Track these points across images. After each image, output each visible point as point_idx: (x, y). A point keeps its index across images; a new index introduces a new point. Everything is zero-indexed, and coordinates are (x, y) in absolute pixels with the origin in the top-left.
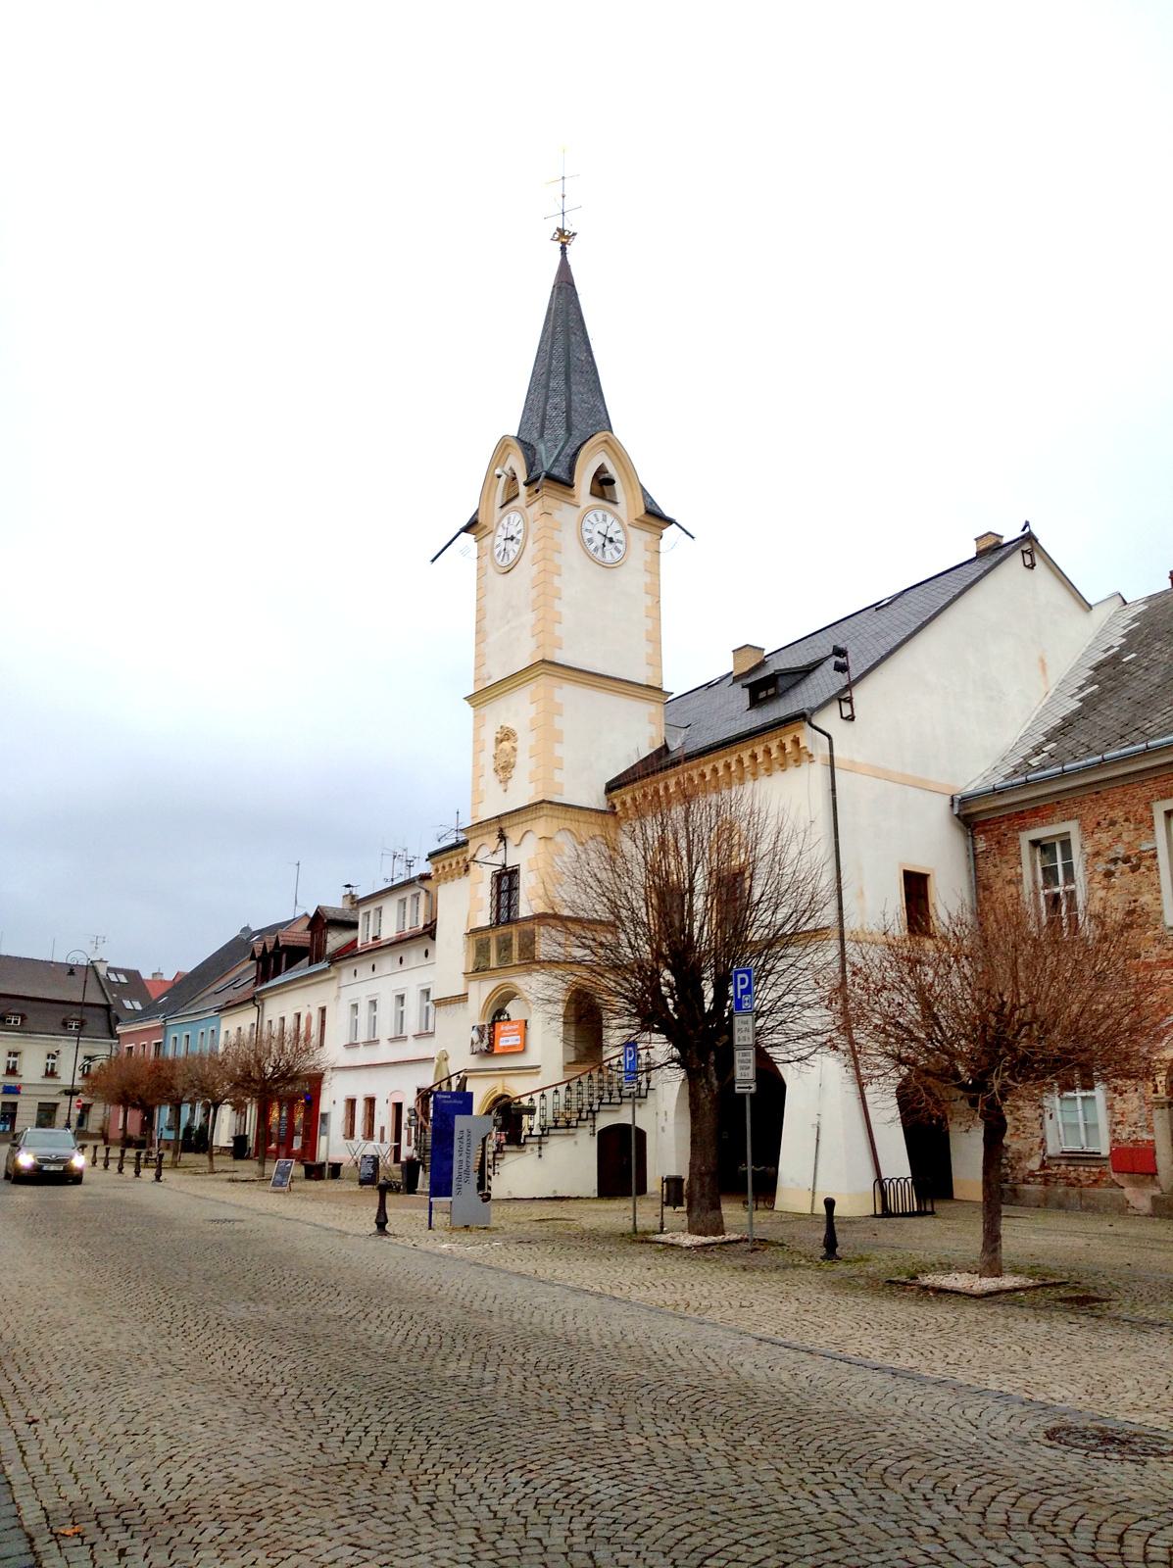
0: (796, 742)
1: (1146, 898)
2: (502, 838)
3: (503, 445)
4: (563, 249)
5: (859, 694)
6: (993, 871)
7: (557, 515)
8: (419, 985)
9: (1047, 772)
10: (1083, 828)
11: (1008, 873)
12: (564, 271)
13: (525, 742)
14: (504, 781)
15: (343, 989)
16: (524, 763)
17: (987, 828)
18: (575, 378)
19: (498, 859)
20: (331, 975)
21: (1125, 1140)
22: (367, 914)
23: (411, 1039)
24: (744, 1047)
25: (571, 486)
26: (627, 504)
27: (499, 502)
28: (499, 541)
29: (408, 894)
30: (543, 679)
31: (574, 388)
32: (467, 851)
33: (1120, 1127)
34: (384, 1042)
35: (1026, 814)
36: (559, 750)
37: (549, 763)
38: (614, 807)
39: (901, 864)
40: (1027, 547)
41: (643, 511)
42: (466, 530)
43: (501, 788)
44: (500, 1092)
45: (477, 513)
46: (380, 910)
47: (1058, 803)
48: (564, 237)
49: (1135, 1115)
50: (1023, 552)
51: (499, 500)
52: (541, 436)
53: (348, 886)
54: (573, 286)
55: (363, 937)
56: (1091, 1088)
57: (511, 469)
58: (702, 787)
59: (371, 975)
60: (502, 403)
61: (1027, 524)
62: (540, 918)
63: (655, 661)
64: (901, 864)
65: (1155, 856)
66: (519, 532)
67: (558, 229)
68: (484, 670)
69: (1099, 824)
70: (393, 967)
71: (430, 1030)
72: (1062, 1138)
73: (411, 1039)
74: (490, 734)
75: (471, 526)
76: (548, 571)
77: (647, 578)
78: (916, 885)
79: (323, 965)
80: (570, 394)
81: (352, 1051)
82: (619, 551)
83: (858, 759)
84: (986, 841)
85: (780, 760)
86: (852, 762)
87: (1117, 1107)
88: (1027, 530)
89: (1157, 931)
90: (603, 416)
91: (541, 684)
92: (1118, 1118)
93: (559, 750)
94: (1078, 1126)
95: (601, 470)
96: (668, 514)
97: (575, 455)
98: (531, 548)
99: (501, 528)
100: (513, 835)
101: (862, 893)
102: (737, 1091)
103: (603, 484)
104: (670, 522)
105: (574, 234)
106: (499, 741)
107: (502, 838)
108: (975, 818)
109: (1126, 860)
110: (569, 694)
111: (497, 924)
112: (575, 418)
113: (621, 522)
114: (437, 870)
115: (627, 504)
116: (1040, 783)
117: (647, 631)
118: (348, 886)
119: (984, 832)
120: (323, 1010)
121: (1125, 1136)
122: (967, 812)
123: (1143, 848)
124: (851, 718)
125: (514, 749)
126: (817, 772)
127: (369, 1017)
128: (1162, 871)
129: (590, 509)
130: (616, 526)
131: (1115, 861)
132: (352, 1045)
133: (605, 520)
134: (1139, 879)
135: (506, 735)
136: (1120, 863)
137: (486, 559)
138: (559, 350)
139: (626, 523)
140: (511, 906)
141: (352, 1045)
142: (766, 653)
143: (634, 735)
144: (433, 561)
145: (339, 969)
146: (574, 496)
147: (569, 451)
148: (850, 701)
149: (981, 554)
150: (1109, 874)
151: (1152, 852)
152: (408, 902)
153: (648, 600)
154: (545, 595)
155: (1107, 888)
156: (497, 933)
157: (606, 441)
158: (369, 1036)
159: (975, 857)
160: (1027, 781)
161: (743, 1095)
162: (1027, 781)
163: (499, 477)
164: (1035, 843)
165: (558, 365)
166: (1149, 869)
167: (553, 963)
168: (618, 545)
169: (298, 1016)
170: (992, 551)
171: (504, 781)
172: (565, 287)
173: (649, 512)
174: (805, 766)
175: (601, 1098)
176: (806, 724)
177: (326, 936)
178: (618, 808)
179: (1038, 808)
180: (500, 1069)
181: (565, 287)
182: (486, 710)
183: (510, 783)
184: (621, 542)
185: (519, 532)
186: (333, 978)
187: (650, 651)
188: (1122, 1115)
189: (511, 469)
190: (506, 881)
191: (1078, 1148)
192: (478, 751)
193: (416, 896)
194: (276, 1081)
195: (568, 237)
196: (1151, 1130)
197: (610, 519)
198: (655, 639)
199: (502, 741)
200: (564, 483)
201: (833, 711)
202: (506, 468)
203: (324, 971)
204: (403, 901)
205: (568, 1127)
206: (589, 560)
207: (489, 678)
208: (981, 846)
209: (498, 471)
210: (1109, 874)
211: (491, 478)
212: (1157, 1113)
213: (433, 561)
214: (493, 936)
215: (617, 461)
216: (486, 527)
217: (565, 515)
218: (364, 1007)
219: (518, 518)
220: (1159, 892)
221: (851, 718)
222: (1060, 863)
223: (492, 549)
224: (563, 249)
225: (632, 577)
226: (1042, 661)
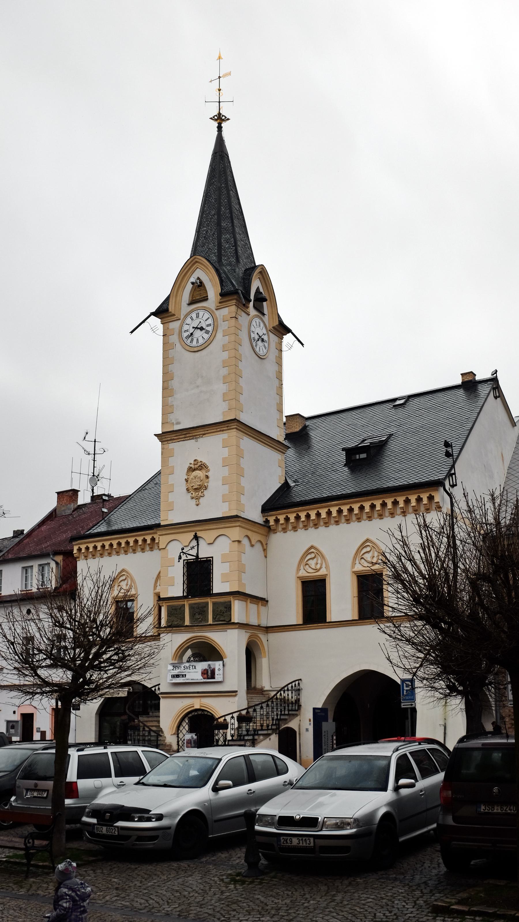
4: (220, 128)
9: (203, 432)
12: (220, 142)
30: (234, 433)
41: (277, 323)
42: (156, 314)
48: (220, 119)
54: (228, 157)
57: (198, 278)
68: (172, 418)
75: (162, 312)
82: (207, 332)
91: (231, 435)
102: (403, 707)
105: (228, 119)
106: (191, 470)
130: (207, 315)
137: (174, 338)
144: (132, 332)
146: (174, 315)
153: (277, 381)
156: (190, 602)
161: (407, 708)
167: (241, 626)
172: (220, 159)
175: (281, 712)
177: (459, 697)
180: (198, 693)
181: (220, 159)
195: (223, 120)
197: (201, 313)
199: (195, 470)
205: (268, 730)
206: (199, 353)
207: (178, 423)
213: (132, 332)
224: (220, 128)
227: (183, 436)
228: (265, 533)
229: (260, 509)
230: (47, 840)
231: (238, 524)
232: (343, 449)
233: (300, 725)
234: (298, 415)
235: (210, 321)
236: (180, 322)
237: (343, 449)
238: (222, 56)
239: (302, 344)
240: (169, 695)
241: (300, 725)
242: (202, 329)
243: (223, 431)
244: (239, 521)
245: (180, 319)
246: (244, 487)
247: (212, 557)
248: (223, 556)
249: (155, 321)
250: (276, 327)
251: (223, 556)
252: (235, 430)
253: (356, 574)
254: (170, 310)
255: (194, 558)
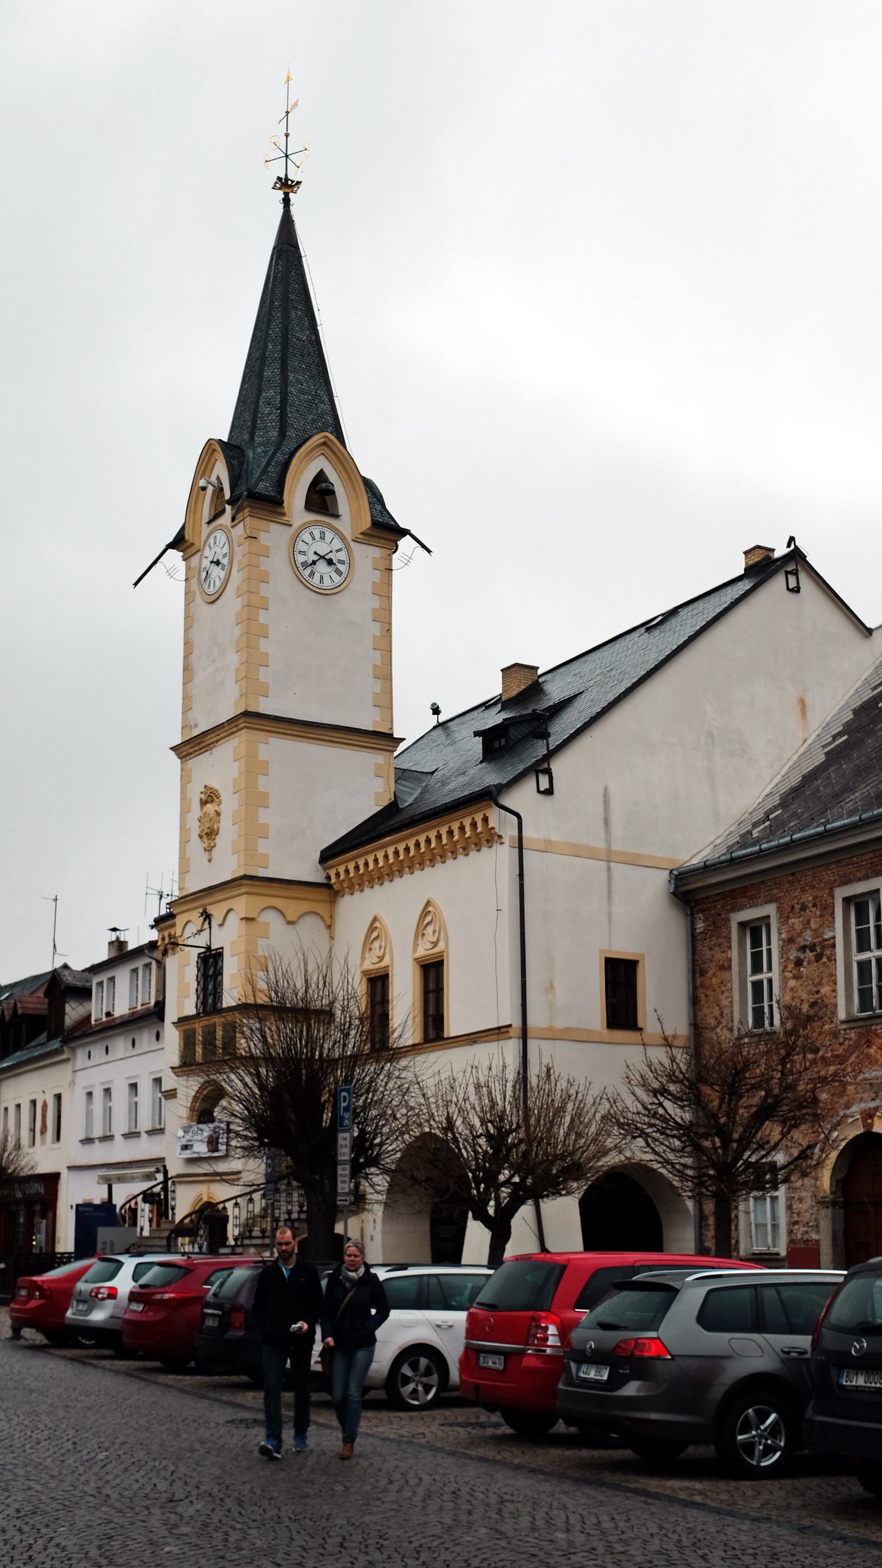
0: (485, 820)
1: (825, 990)
2: (207, 917)
3: (210, 447)
4: (286, 201)
5: (558, 766)
6: (708, 954)
7: (263, 537)
8: (151, 1073)
10: (780, 910)
11: (719, 956)
12: (287, 225)
13: (229, 804)
14: (209, 850)
15: (78, 1073)
16: (228, 830)
17: (705, 906)
18: (293, 363)
19: (202, 940)
20: (65, 1056)
21: (799, 1241)
22: (100, 984)
23: (144, 1136)
24: (344, 1163)
25: (280, 503)
26: (351, 512)
27: (206, 516)
28: (206, 563)
29: (139, 963)
31: (291, 376)
32: (174, 925)
33: (796, 1227)
34: (118, 1138)
35: (743, 892)
36: (264, 816)
37: (254, 832)
38: (328, 878)
39: (601, 951)
40: (791, 567)
41: (369, 524)
42: (171, 546)
43: (206, 856)
44: (205, 1199)
45: (183, 528)
46: (112, 979)
47: (762, 883)
48: (286, 185)
49: (808, 1215)
50: (787, 573)
51: (206, 514)
52: (252, 438)
53: (114, 930)
55: (96, 1010)
56: (776, 1189)
58: (407, 863)
59: (105, 1059)
60: (211, 398)
61: (792, 539)
62: (243, 1008)
63: (385, 702)
64: (601, 951)
65: (834, 946)
66: (225, 556)
67: (279, 179)
69: (793, 907)
70: (126, 1050)
71: (162, 1126)
72: (754, 1238)
73: (144, 1136)
74: (196, 794)
75: (178, 542)
76: (255, 605)
77: (376, 603)
78: (621, 977)
79: (55, 1044)
80: (286, 386)
81: (88, 1147)
82: (339, 573)
83: (555, 837)
84: (704, 921)
85: (474, 840)
86: (549, 842)
87: (794, 1207)
88: (792, 547)
89: (832, 1025)
90: (325, 407)
92: (796, 1218)
93: (264, 816)
94: (765, 1225)
95: (321, 477)
96: (403, 525)
97: (286, 465)
98: (237, 577)
99: (207, 548)
100: (217, 912)
101: (552, 986)
103: (321, 498)
104: (405, 532)
105: (299, 183)
106: (204, 803)
107: (207, 917)
108: (700, 895)
109: (812, 948)
110: (277, 748)
111: (205, 1012)
112: (292, 417)
113: (343, 538)
114: (163, 939)
115: (351, 512)
116: (801, 844)
117: (374, 666)
118: (114, 930)
119: (703, 911)
120: (58, 1097)
121: (799, 1237)
122: (684, 889)
123: (826, 937)
124: (549, 792)
125: (218, 814)
126: (503, 855)
127: (130, 1106)
128: (838, 962)
129: (305, 526)
130: (337, 544)
131: (803, 949)
132: (88, 1141)
133: (322, 538)
134: (822, 969)
135: (210, 796)
136: (808, 951)
137: (194, 582)
138: (275, 329)
139: (349, 538)
140: (217, 993)
141: (88, 1141)
142: (540, 672)
143: (358, 788)
145: (73, 1050)
146: (284, 514)
147: (280, 457)
148: (548, 772)
149: (750, 571)
150: (799, 963)
151: (832, 941)
152: (140, 972)
153: (376, 629)
154: (252, 632)
155: (797, 977)
157: (324, 444)
158: (104, 1132)
159: (694, 940)
160: (761, 850)
162: (826, 831)
163: (204, 489)
164: (743, 925)
165: (273, 349)
166: (829, 959)
168: (340, 566)
169: (34, 1102)
170: (763, 567)
171: (209, 850)
173: (375, 524)
174: (496, 846)
176: (492, 803)
178: (333, 880)
179: (745, 887)
180: (205, 1175)
182: (193, 763)
183: (214, 851)
184: (342, 562)
185: (225, 556)
186: (67, 1060)
187: (378, 690)
188: (798, 1214)
189: (218, 478)
190: (211, 962)
191: (763, 1249)
192: (184, 812)
193: (148, 966)
194: (274, 1169)
196: (818, 1232)
197: (329, 535)
198: (384, 675)
199: (206, 803)
200: (270, 503)
201: (529, 786)
202: (213, 479)
203: (57, 1052)
204: (135, 971)
205: (263, 1237)
206: (302, 587)
207: (196, 726)
208: (700, 926)
209: (202, 483)
210: (799, 963)
211: (196, 492)
212: (823, 1212)
214: (198, 1026)
215: (340, 467)
216: (192, 544)
217: (274, 536)
218: (98, 1095)
219: (224, 539)
220: (835, 983)
221: (549, 792)
222: (764, 948)
223: (200, 571)
224: (286, 201)
225: (357, 603)
226: (802, 703)
227: (197, 748)
228: (328, 899)
229: (317, 856)
230: (512, 1427)
231: (243, 890)
232: (476, 734)
233: (362, 1229)
234: (516, 665)
235: (342, 555)
236: (291, 531)
237: (476, 734)
238: (292, 76)
239: (429, 551)
240: (183, 1178)
241: (362, 1229)
242: (330, 562)
243: (233, 733)
244: (243, 885)
245: (291, 525)
246: (267, 825)
247: (222, 948)
248: (233, 943)
249: (174, 556)
250: (369, 532)
251: (233, 943)
252: (244, 730)
253: (418, 963)
254: (187, 538)
255: (203, 950)
